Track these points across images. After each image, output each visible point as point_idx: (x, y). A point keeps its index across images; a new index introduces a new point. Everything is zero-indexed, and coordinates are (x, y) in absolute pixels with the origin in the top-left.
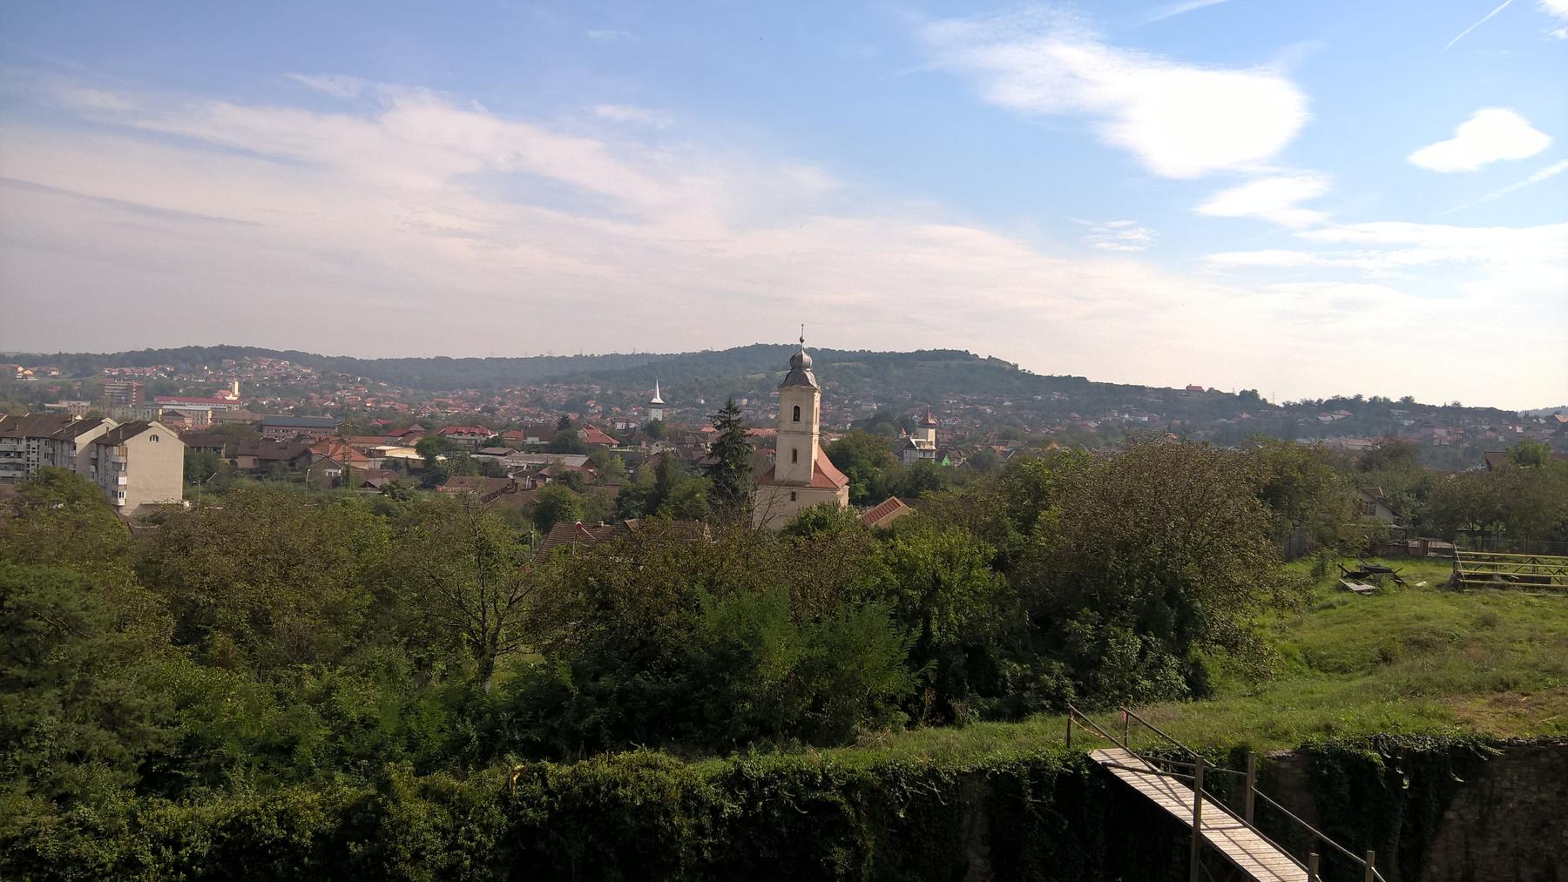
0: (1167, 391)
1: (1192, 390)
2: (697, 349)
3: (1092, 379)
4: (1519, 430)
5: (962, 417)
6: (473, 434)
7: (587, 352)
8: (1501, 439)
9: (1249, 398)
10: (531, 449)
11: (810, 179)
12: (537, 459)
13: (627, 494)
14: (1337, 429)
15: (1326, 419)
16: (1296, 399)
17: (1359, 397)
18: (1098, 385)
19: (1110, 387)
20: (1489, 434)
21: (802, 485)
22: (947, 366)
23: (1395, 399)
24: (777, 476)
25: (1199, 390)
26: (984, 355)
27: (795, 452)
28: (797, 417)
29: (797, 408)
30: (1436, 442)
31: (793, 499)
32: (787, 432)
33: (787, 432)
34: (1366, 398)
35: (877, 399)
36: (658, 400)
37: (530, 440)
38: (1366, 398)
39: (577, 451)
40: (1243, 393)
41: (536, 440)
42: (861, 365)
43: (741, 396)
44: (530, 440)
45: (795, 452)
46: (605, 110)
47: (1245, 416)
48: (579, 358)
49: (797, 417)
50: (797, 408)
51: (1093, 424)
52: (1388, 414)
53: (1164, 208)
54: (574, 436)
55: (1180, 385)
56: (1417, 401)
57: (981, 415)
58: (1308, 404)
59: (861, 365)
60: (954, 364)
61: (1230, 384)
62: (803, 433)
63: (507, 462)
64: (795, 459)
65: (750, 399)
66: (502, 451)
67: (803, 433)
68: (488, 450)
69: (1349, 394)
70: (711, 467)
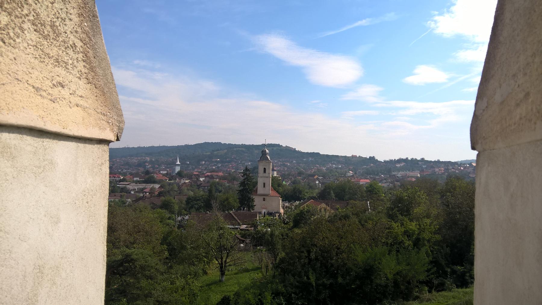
0: (346, 157)
1: (353, 157)
2: (183, 143)
3: (321, 153)
4: (462, 168)
5: (280, 166)
6: (115, 177)
7: (142, 146)
8: (457, 171)
9: (372, 159)
10: (137, 182)
11: (209, 86)
12: (141, 186)
13: (190, 199)
14: (401, 169)
15: (398, 165)
16: (387, 159)
17: (407, 158)
18: (324, 155)
19: (327, 156)
20: (453, 170)
21: (267, 195)
22: (273, 149)
23: (419, 159)
24: (258, 193)
25: (356, 157)
26: (284, 146)
27: (264, 184)
28: (265, 171)
29: (265, 169)
30: (437, 173)
31: (264, 200)
32: (261, 177)
33: (261, 177)
34: (409, 159)
35: (250, 161)
36: (178, 163)
37: (135, 179)
38: (409, 159)
39: (155, 182)
40: (370, 157)
41: (138, 179)
42: (243, 149)
43: (202, 161)
44: (135, 179)
45: (264, 184)
46: (136, 62)
47: (372, 165)
48: (139, 148)
49: (265, 171)
50: (265, 169)
51: (324, 169)
52: (418, 164)
53: (333, 97)
54: (153, 177)
55: (349, 155)
56: (426, 159)
57: (286, 166)
58: (391, 161)
59: (243, 149)
60: (275, 148)
61: (366, 155)
62: (267, 177)
63: (130, 187)
64: (264, 186)
65: (205, 162)
66: (128, 183)
67: (267, 177)
68: (121, 183)
69: (404, 157)
70: (240, 191)
